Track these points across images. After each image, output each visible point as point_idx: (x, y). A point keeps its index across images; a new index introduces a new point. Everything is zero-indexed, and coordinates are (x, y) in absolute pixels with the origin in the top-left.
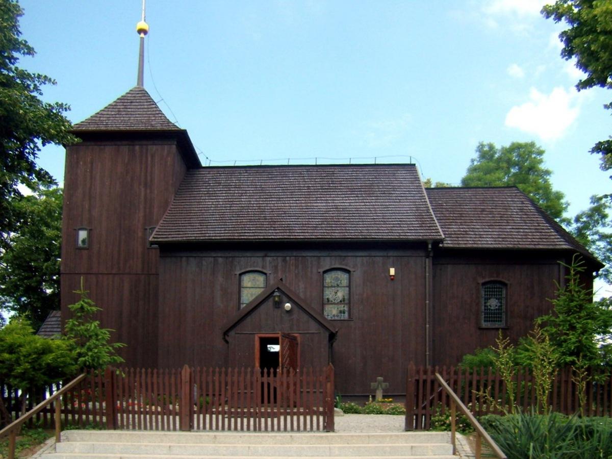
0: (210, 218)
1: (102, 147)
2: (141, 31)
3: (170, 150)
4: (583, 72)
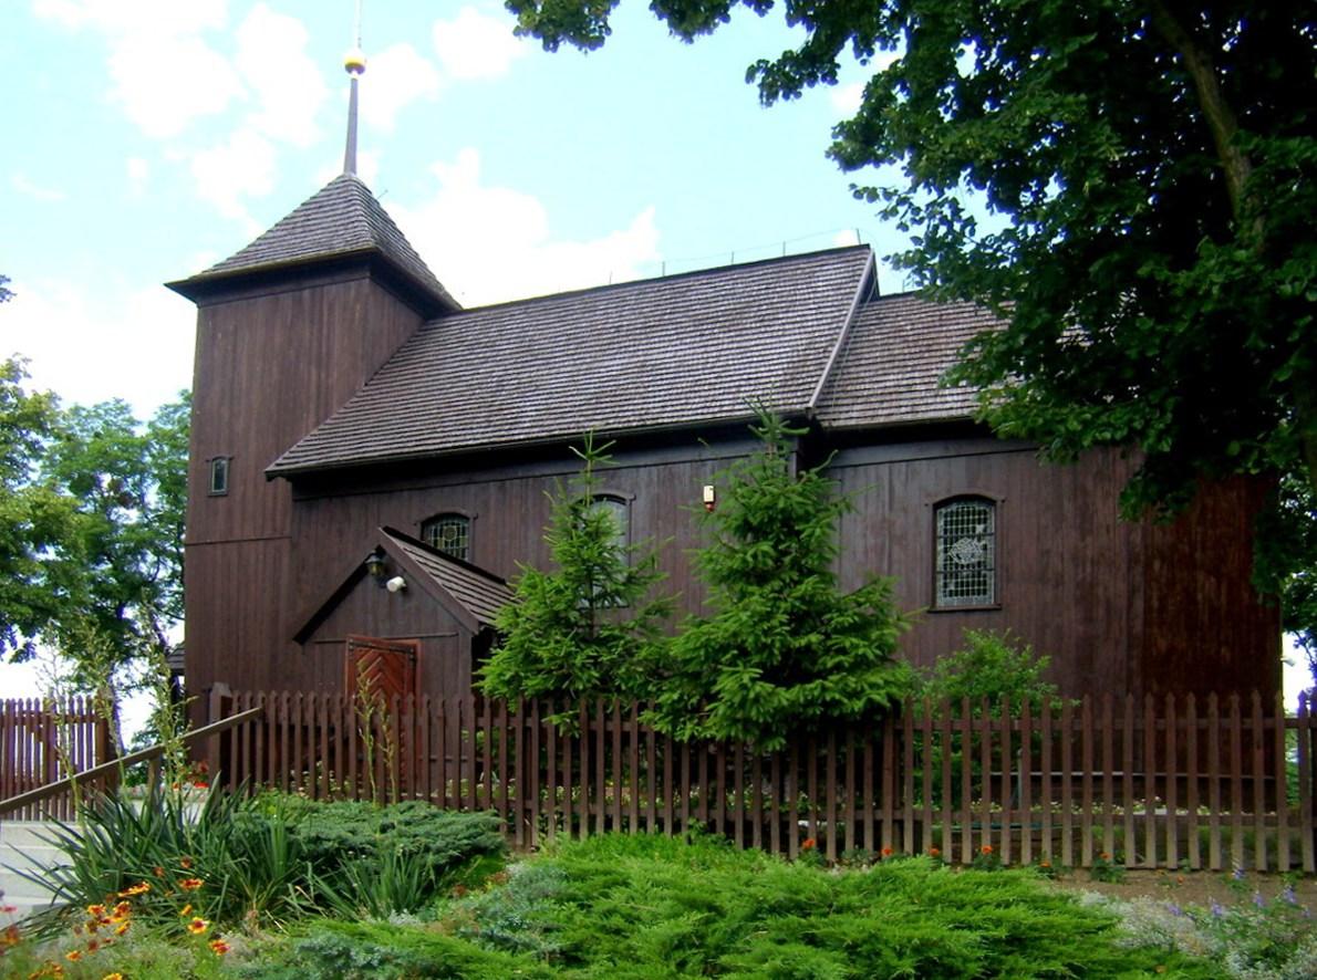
0: (436, 410)
1: (252, 301)
2: (351, 67)
3: (358, 292)
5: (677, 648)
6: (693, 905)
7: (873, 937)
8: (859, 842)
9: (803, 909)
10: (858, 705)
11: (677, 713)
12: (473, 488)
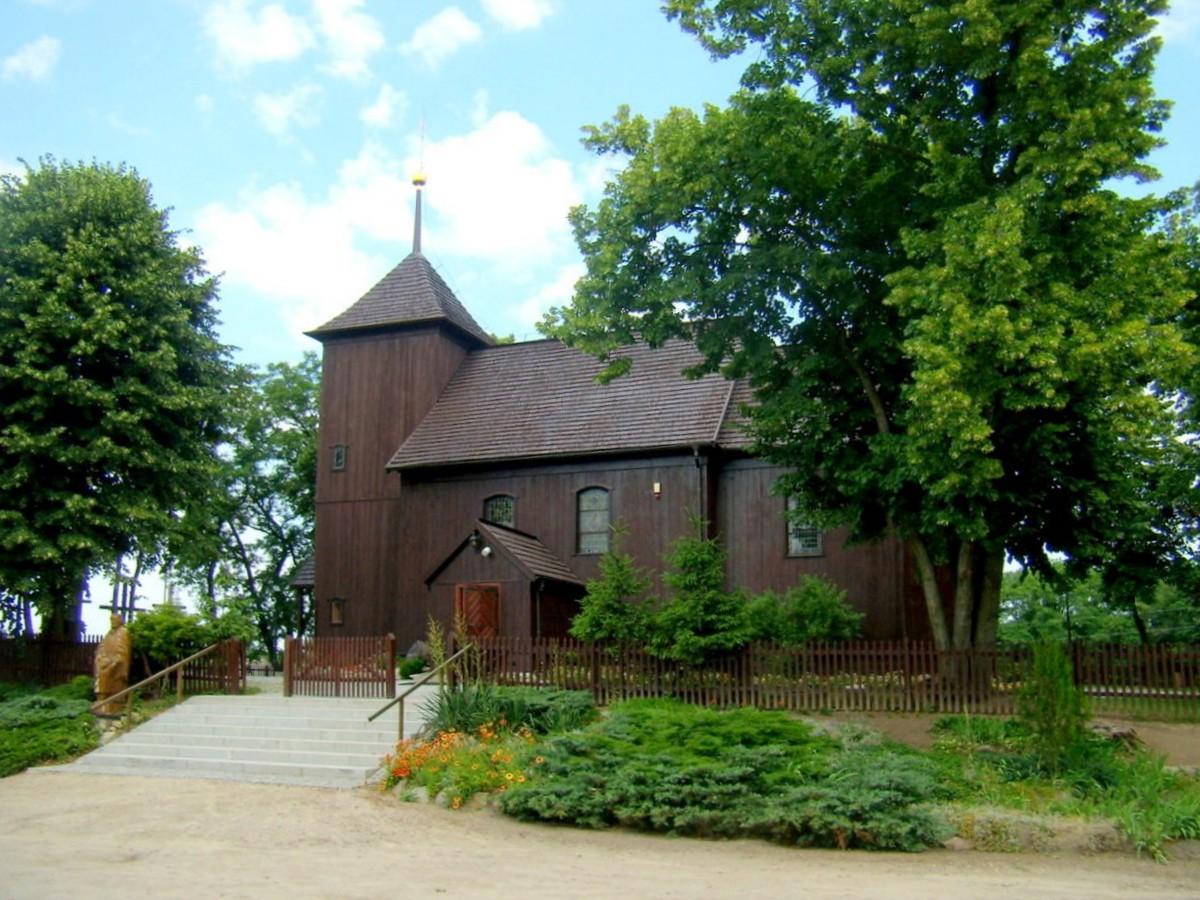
2: (416, 183)
3: (433, 341)
4: (1168, 130)
5: (660, 619)
6: (674, 724)
7: (730, 732)
8: (734, 701)
9: (709, 724)
10: (731, 645)
11: (660, 647)
12: (515, 480)
